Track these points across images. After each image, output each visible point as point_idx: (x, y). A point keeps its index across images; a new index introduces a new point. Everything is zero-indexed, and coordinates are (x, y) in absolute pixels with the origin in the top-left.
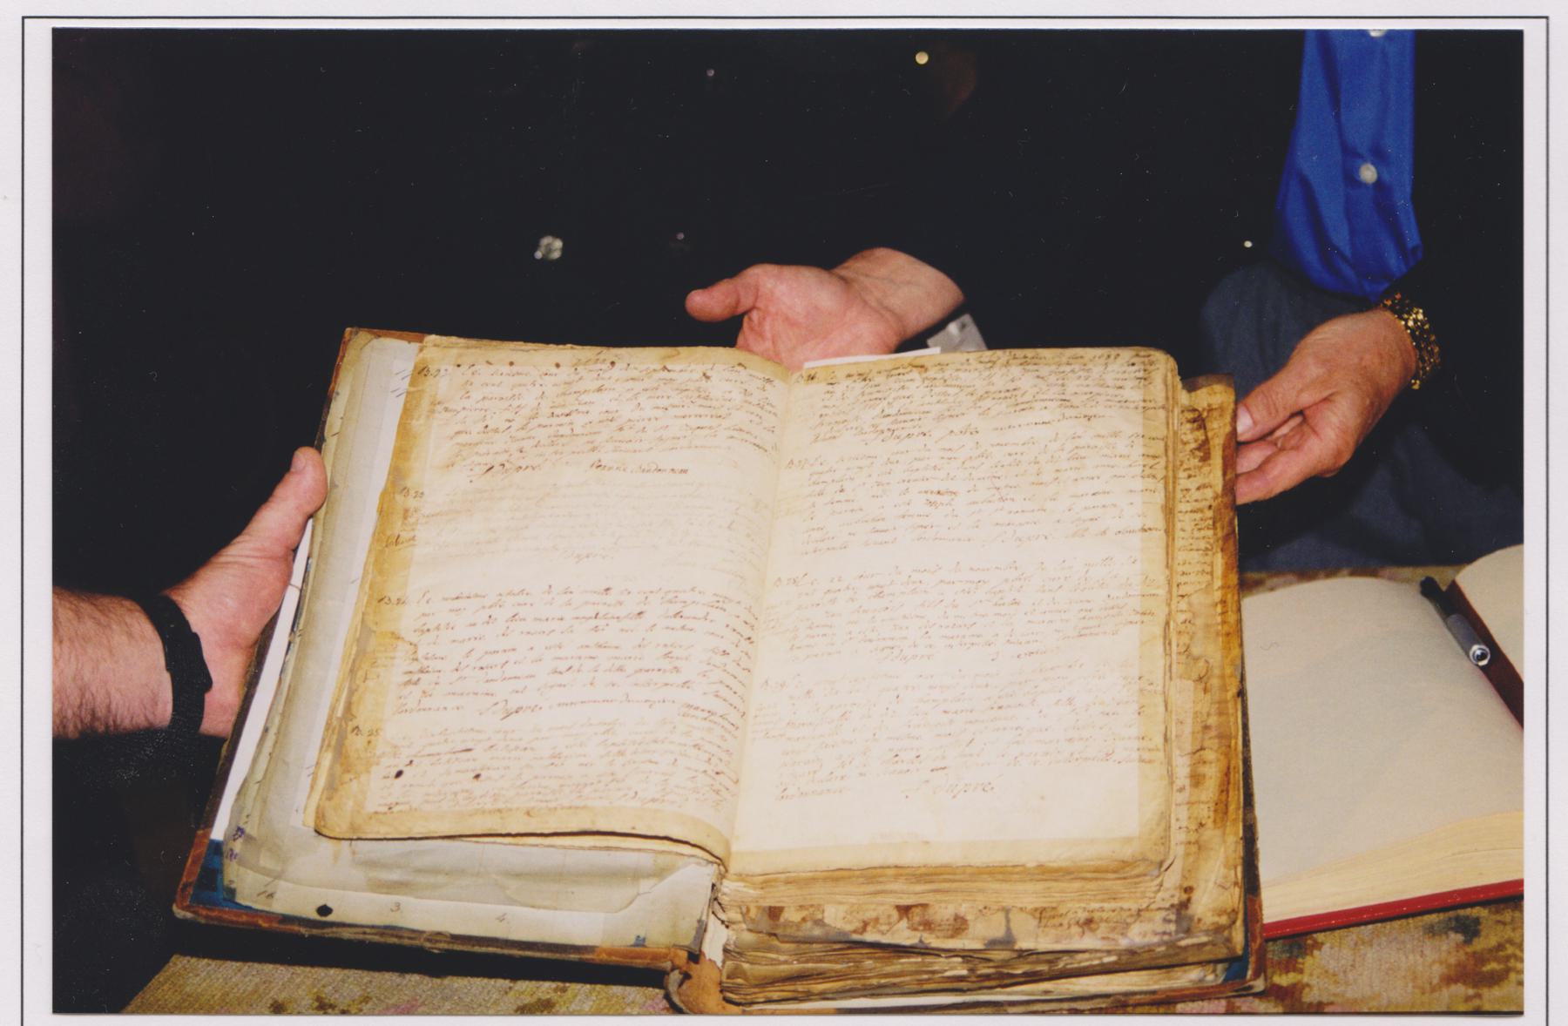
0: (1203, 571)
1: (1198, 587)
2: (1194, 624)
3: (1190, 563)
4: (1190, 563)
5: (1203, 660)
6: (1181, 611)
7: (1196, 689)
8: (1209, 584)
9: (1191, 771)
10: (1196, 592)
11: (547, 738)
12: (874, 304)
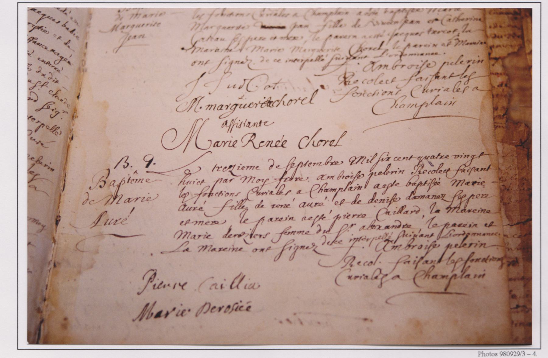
0: (514, 34)
1: (511, 50)
2: (510, 88)
3: (501, 27)
4: (501, 27)
5: (523, 125)
6: (497, 74)
7: (518, 154)
8: (521, 47)
9: (523, 242)
10: (509, 54)
11: (46, 289)
12: (467, 265)
